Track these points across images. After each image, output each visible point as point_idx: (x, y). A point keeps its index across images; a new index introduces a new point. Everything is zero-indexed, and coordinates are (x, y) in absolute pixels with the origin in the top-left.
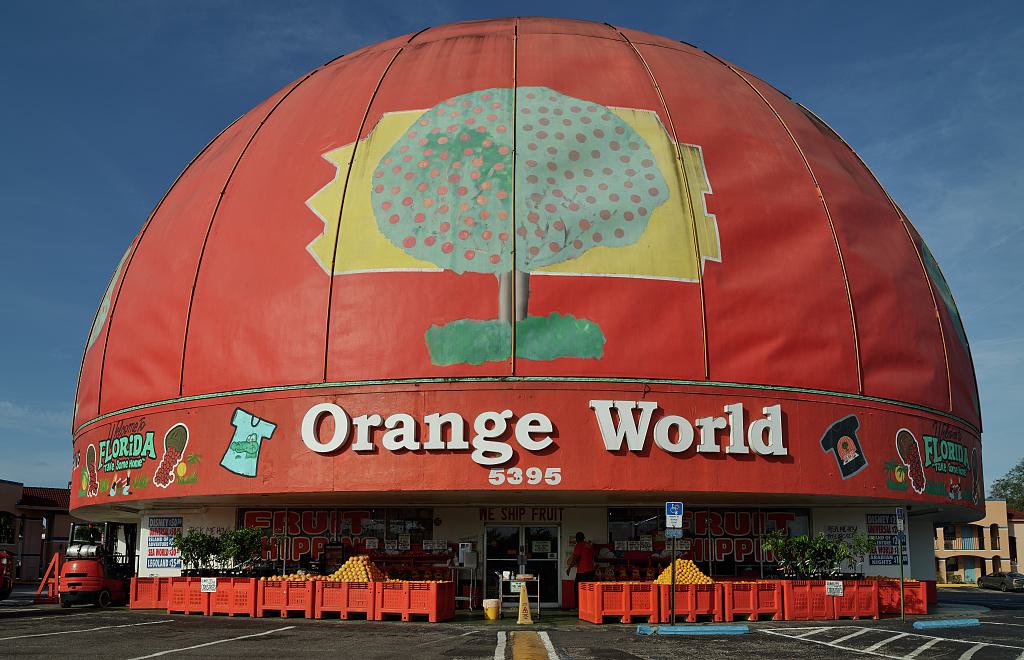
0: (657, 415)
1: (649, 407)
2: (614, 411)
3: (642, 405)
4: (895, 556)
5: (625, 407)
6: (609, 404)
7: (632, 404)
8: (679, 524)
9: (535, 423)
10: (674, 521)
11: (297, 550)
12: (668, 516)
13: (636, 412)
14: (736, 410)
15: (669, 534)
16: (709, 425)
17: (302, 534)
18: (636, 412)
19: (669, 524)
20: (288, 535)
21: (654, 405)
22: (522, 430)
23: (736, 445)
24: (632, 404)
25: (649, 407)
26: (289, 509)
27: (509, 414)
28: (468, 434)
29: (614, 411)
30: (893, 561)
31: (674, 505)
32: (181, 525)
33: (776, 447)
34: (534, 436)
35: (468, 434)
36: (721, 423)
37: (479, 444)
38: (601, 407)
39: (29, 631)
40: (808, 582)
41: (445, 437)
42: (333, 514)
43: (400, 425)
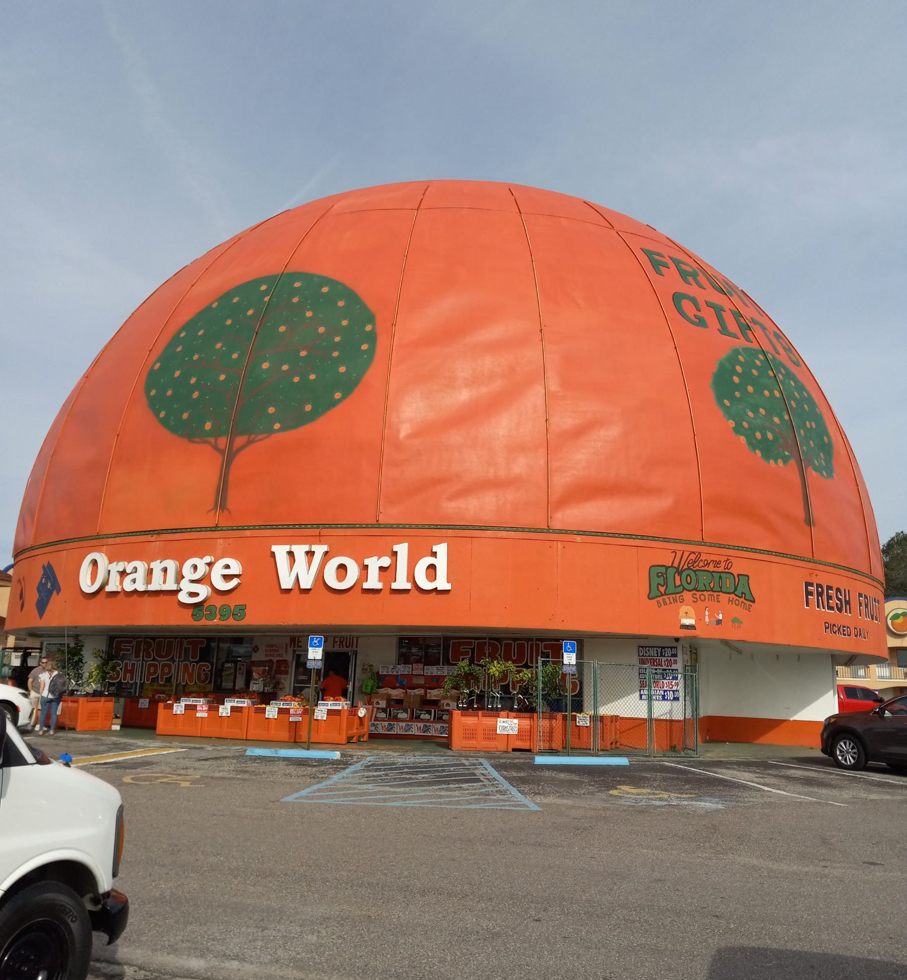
0: (327, 556)
1: (319, 550)
2: (291, 554)
3: (315, 548)
4: (665, 691)
5: (300, 550)
6: (287, 548)
7: (306, 548)
8: (573, 662)
9: (227, 567)
10: (315, 654)
11: (149, 674)
12: (310, 649)
13: (310, 554)
14: (402, 549)
15: (566, 670)
16: (374, 564)
17: (154, 659)
18: (310, 554)
19: (566, 661)
20: (143, 660)
21: (325, 548)
22: (217, 572)
23: (401, 583)
24: (306, 548)
25: (319, 550)
26: (490, 639)
27: (208, 559)
28: (180, 577)
29: (291, 554)
30: (663, 696)
31: (316, 639)
32: (676, 655)
33: (442, 583)
34: (227, 578)
35: (180, 577)
36: (386, 561)
37: (186, 587)
38: (280, 551)
39: (75, 744)
40: (103, 698)
41: (149, 580)
42: (532, 645)
43: (135, 570)
